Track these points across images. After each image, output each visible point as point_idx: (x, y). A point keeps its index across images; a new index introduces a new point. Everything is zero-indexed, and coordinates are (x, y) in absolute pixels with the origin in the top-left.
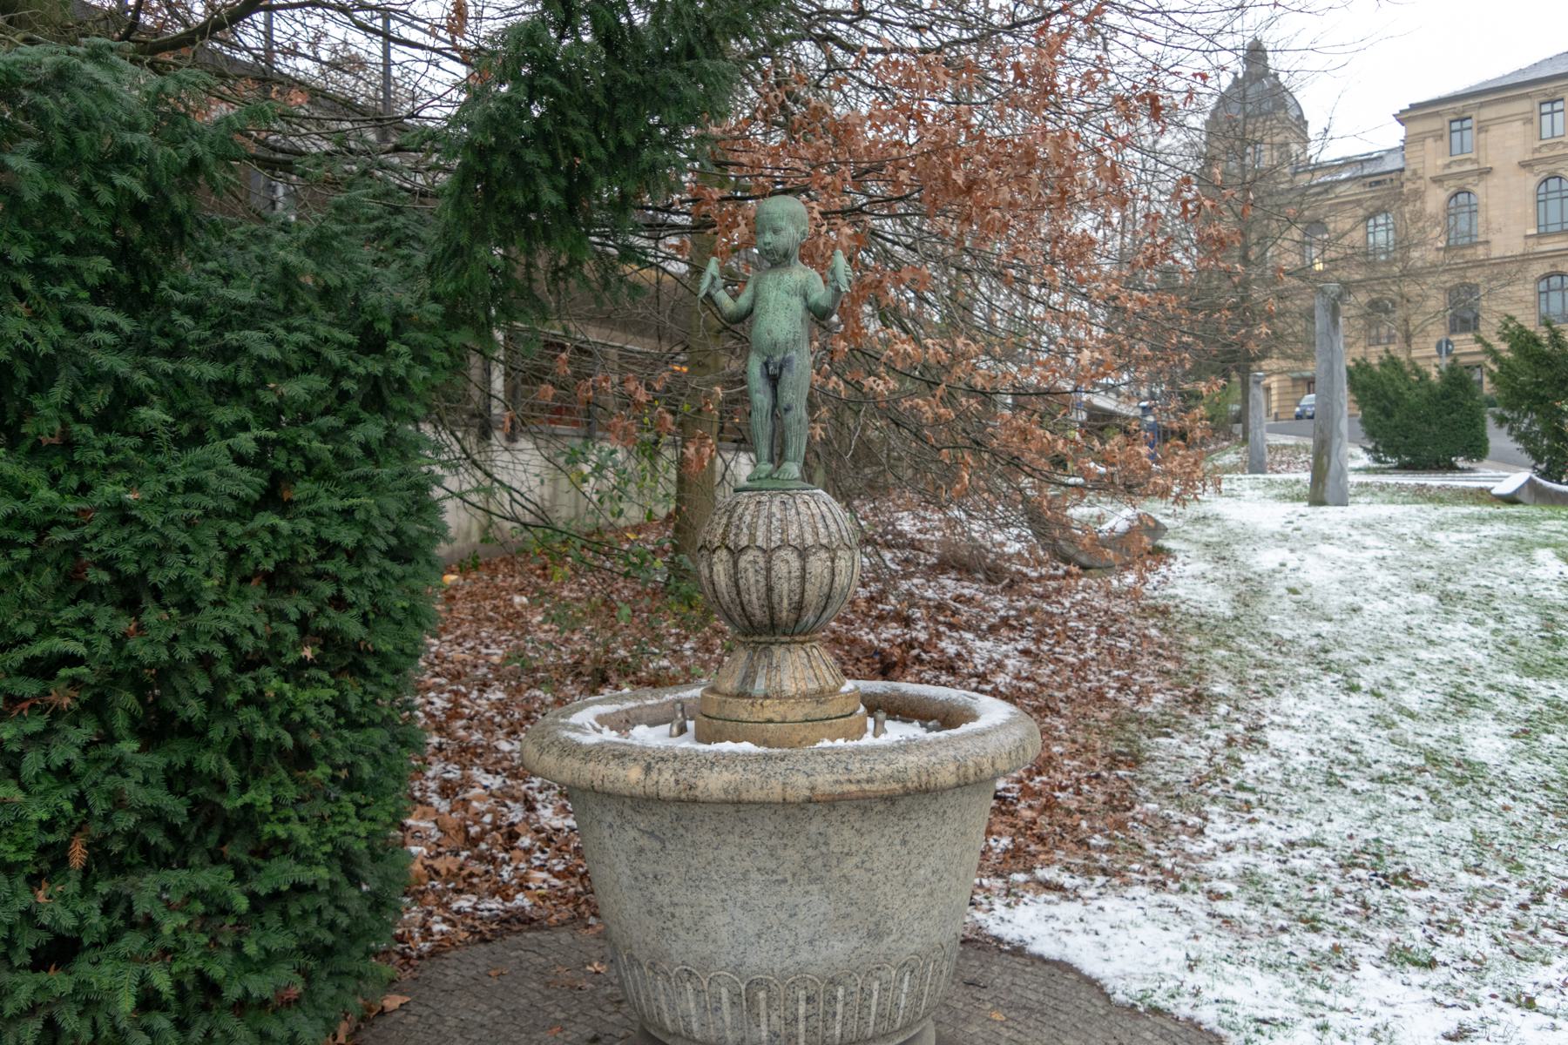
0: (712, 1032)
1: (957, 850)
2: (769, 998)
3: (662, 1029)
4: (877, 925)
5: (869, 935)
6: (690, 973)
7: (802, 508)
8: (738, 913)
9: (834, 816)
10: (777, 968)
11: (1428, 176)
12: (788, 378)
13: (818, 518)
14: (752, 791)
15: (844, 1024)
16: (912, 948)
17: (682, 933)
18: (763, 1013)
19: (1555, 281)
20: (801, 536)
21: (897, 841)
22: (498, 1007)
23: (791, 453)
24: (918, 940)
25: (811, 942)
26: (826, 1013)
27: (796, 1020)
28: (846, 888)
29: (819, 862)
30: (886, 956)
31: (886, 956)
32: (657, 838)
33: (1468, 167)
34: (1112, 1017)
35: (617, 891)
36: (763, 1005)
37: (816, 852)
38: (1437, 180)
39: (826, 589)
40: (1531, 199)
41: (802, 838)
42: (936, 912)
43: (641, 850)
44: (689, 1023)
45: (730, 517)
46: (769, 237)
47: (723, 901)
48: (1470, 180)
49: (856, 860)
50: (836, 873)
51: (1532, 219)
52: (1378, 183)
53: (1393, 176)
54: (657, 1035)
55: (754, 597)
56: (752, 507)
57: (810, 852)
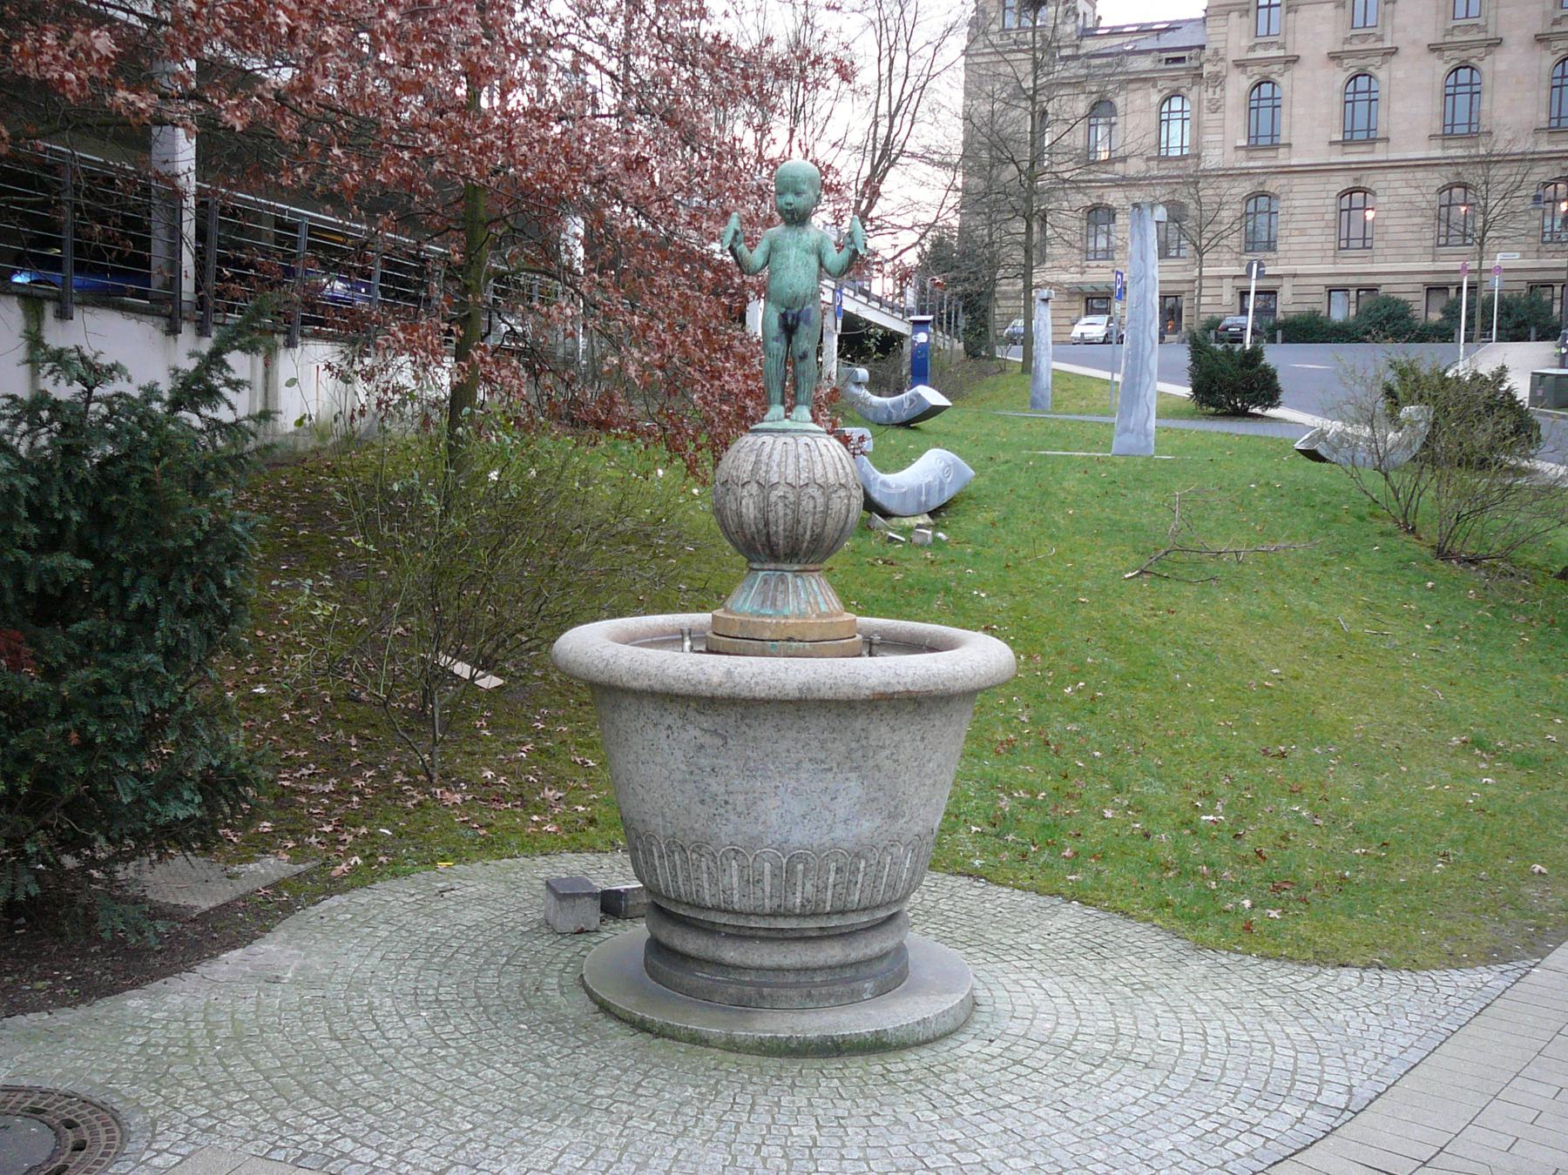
2: (805, 869)
4: (896, 808)
6: (737, 852)
7: (824, 450)
9: (875, 715)
11: (1230, 58)
15: (862, 891)
16: (916, 830)
17: (733, 817)
18: (799, 883)
19: (1358, 196)
20: (825, 475)
21: (918, 738)
23: (801, 397)
24: (921, 823)
26: (850, 881)
28: (877, 775)
29: (860, 753)
33: (1273, 52)
36: (800, 875)
38: (1240, 65)
39: (842, 523)
40: (1338, 98)
43: (702, 746)
48: (1276, 68)
49: (888, 752)
50: (871, 763)
51: (1337, 122)
52: (1181, 60)
53: (1194, 52)
57: (853, 745)
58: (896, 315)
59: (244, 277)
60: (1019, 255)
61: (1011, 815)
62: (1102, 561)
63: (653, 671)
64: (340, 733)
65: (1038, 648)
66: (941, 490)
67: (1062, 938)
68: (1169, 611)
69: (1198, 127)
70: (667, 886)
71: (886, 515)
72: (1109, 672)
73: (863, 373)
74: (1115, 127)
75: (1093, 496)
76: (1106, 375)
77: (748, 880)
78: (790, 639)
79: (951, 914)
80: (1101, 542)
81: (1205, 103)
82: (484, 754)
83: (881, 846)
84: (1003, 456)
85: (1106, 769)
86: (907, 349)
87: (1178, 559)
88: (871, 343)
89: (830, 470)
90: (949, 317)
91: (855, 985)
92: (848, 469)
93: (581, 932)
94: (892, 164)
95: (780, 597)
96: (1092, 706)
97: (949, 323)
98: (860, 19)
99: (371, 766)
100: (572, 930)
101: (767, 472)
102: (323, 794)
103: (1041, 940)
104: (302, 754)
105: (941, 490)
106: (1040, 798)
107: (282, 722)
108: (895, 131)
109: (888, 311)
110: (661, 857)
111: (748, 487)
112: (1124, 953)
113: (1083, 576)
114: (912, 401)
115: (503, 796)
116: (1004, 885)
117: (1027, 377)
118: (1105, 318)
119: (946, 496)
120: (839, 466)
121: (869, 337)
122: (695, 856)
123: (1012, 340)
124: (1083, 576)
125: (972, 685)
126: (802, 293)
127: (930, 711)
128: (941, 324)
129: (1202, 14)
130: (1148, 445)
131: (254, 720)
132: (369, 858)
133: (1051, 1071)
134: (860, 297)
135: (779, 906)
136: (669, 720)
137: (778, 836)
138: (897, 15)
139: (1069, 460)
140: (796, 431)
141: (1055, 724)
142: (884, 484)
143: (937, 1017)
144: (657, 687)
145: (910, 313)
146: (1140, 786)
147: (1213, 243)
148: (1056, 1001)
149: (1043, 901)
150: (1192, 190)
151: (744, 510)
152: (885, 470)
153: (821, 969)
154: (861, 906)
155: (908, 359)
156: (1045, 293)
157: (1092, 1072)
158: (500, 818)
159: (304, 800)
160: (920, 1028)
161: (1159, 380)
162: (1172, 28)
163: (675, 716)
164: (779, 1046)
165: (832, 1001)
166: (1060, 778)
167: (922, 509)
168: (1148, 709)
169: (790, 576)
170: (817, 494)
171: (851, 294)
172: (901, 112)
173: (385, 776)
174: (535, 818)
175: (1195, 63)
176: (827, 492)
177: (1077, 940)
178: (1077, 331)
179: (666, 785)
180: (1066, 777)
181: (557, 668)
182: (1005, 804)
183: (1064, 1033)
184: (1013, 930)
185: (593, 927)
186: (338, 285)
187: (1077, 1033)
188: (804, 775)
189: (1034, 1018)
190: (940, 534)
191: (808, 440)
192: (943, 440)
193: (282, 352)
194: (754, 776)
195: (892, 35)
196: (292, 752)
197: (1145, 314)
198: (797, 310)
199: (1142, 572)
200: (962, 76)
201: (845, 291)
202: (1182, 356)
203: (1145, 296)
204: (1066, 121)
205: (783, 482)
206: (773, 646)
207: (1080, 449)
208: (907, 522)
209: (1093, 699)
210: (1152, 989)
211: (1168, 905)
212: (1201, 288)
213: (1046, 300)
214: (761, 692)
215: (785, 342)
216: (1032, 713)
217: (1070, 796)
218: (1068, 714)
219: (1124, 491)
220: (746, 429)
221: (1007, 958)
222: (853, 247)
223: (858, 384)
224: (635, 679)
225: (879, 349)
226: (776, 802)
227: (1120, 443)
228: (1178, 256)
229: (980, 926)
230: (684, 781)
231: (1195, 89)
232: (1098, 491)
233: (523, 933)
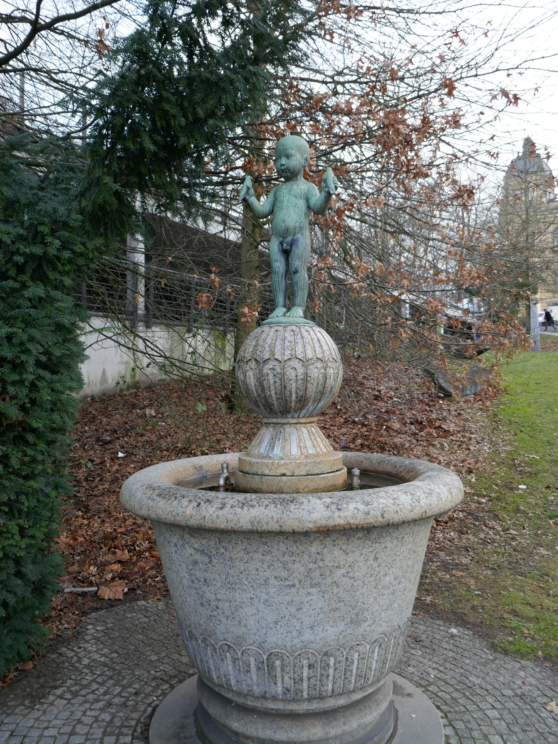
0: (244, 686)
1: (410, 563)
3: (212, 681)
4: (357, 615)
5: (352, 622)
6: (229, 647)
7: (305, 334)
8: (261, 607)
10: (289, 645)
12: (296, 251)
13: (316, 340)
14: (271, 524)
16: (380, 630)
17: (223, 620)
18: (279, 675)
21: (371, 558)
22: (116, 652)
24: (384, 624)
25: (312, 628)
26: (322, 675)
27: (302, 680)
28: (336, 590)
29: (318, 573)
30: (363, 636)
31: (363, 636)
32: (206, 554)
34: (497, 662)
35: (181, 588)
36: (279, 670)
39: (320, 388)
41: (306, 557)
42: (396, 605)
43: (196, 562)
44: (229, 680)
45: (257, 341)
46: (284, 161)
47: (251, 598)
49: (343, 571)
50: (329, 580)
54: (209, 684)
55: (273, 393)
56: (272, 334)
57: (311, 566)
77: (239, 670)
92: (325, 348)
111: (250, 363)
120: (317, 345)
137: (257, 638)
151: (248, 380)
154: (336, 692)
163: (178, 536)
176: (306, 364)
188: (272, 590)
194: (234, 588)
222: (326, 189)
226: (252, 611)
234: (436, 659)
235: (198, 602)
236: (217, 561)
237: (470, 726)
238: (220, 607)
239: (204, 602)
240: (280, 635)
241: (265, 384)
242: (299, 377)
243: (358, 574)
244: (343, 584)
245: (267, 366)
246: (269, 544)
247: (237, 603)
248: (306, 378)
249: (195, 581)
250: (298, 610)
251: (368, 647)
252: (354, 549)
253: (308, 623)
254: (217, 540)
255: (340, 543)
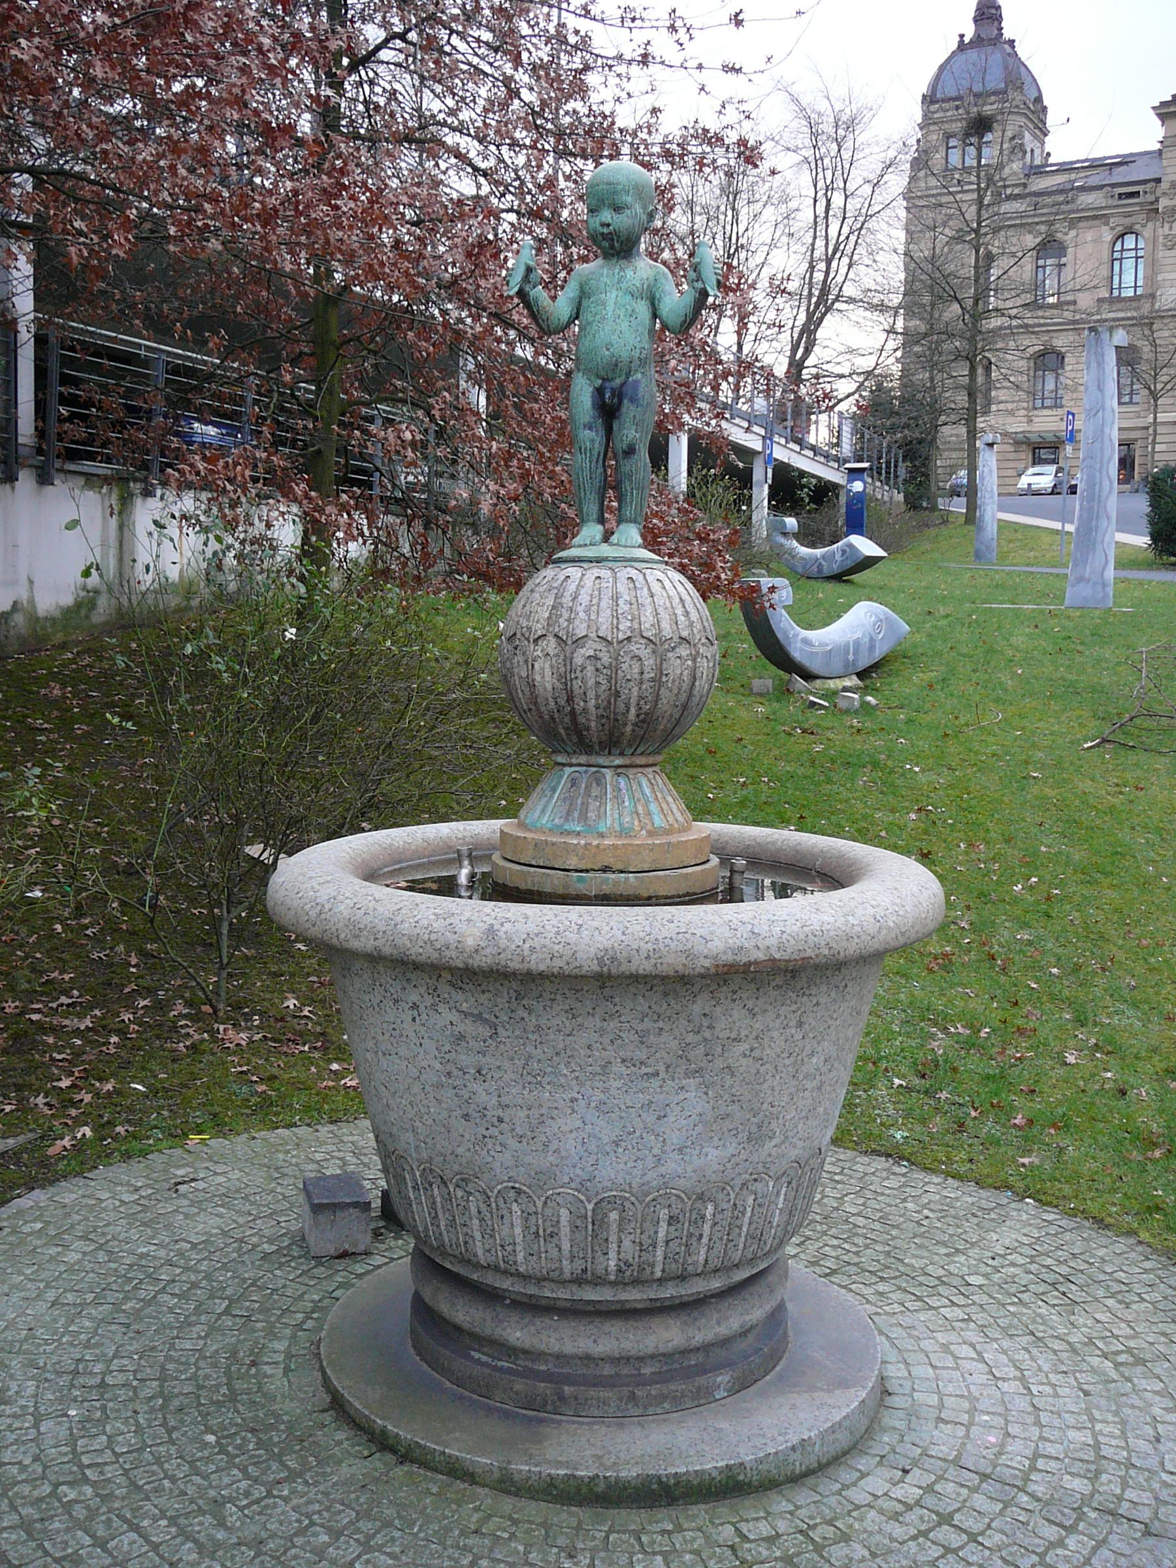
2: (622, 1219)
4: (760, 1127)
5: (749, 1140)
6: (519, 1192)
7: (656, 588)
8: (592, 1114)
14: (635, 963)
16: (794, 1153)
17: (512, 1143)
18: (613, 1238)
21: (793, 1023)
24: (800, 1144)
27: (654, 1246)
28: (728, 1081)
29: (701, 1050)
32: (486, 1021)
36: (614, 1227)
37: (698, 1038)
39: (683, 697)
43: (461, 1037)
49: (744, 1047)
50: (719, 1063)
53: (1149, 185)
57: (690, 1038)
58: (831, 464)
59: (84, 418)
60: (962, 399)
61: (946, 1061)
62: (1056, 728)
63: (381, 926)
64: (121, 948)
65: (982, 835)
66: (872, 648)
67: (1013, 1264)
68: (1137, 788)
69: (1154, 267)
70: (426, 1229)
71: (808, 676)
72: (1067, 864)
73: (791, 522)
74: (1064, 270)
75: (1044, 654)
76: (1057, 525)
77: (537, 1234)
78: (605, 869)
79: (860, 1221)
80: (1055, 706)
81: (1161, 239)
82: (292, 975)
83: (738, 1182)
84: (942, 610)
85: (1066, 993)
86: (843, 500)
87: (1145, 725)
88: (804, 494)
89: (665, 617)
90: (888, 467)
91: (701, 1380)
92: (694, 616)
93: (344, 1255)
94: (828, 309)
95: (593, 805)
96: (1046, 908)
97: (888, 473)
98: (796, 158)
99: (150, 992)
100: (332, 1252)
101: (569, 620)
102: (77, 1032)
103: (983, 1269)
104: (67, 977)
105: (872, 648)
106: (982, 1035)
107: (52, 935)
108: (832, 275)
109: (822, 459)
110: (416, 1188)
112: (1101, 1293)
113: (1034, 746)
114: (844, 552)
115: (301, 1035)
116: (933, 1171)
117: (971, 528)
118: (1052, 468)
119: (878, 655)
120: (679, 611)
121: (803, 487)
122: (460, 1193)
123: (955, 492)
124: (1034, 746)
125: (876, 945)
126: (625, 355)
127: (811, 982)
128: (879, 473)
129: (1158, 146)
130: (1106, 596)
131: (17, 933)
132: (103, 1128)
133: (998, 1538)
134: (792, 445)
135: (584, 1271)
136: (414, 997)
137: (578, 1171)
138: (833, 154)
139: (1017, 614)
140: (615, 560)
141: (1001, 930)
142: (805, 641)
143: (822, 1436)
144: (387, 950)
145: (846, 461)
146: (1109, 1016)
147: (1169, 386)
148: (1005, 1386)
149: (986, 1197)
150: (1147, 332)
151: (538, 678)
152: (810, 626)
153: (652, 1357)
154: (711, 1266)
155: (843, 510)
156: (989, 438)
157: (1061, 1543)
158: (289, 1066)
159: (51, 1040)
160: (797, 1456)
161: (1118, 530)
162: (1126, 161)
163: (422, 990)
164: (579, 1490)
165: (666, 1405)
166: (1007, 1005)
167: (851, 670)
168: (1116, 910)
169: (608, 773)
170: (645, 652)
171: (783, 441)
172: (838, 255)
173: (161, 1007)
174: (335, 1066)
175: (1150, 198)
176: (660, 649)
177: (1033, 1267)
178: (1024, 481)
179: (416, 1089)
180: (1016, 1004)
181: (265, 912)
182: (939, 1045)
183: (1017, 1455)
184: (943, 1251)
185: (361, 1248)
186: (212, 431)
187: (1036, 1456)
189: (971, 1423)
190: (869, 698)
191: (633, 573)
192: (875, 594)
193: (138, 501)
195: (829, 174)
196: (56, 974)
197: (1102, 449)
198: (618, 381)
199: (1104, 741)
200: (903, 214)
201: (776, 438)
202: (1141, 504)
203: (1102, 431)
204: (1013, 255)
205: (593, 635)
206: (580, 879)
207: (1029, 602)
208: (832, 684)
209: (1048, 899)
210: (1143, 1362)
211: (1158, 1209)
212: (1155, 433)
213: (991, 445)
214: (537, 963)
215: (602, 432)
216: (974, 917)
217: (1021, 1031)
218: (1018, 918)
219: (1080, 648)
220: (551, 561)
221: (933, 1302)
222: (699, 285)
223: (785, 534)
224: (356, 937)
225: (813, 500)
227: (1074, 594)
228: (1131, 402)
229: (898, 1243)
230: (439, 1086)
231: (1150, 225)
232: (1050, 649)
233: (266, 1256)
234: (833, 1231)
235: (458, 1112)
236: (509, 1033)
237: (916, 1333)
238: (507, 1119)
239: (471, 1112)
240: (622, 1166)
241: (576, 687)
242: (646, 676)
243: (768, 1051)
244: (741, 1070)
245: (582, 651)
246: (617, 1000)
247: (543, 1111)
248: (658, 681)
249: (455, 1072)
250: (659, 1118)
251: (771, 1184)
252: (767, 1006)
253: (675, 1141)
254: (514, 995)
255: (744, 996)
